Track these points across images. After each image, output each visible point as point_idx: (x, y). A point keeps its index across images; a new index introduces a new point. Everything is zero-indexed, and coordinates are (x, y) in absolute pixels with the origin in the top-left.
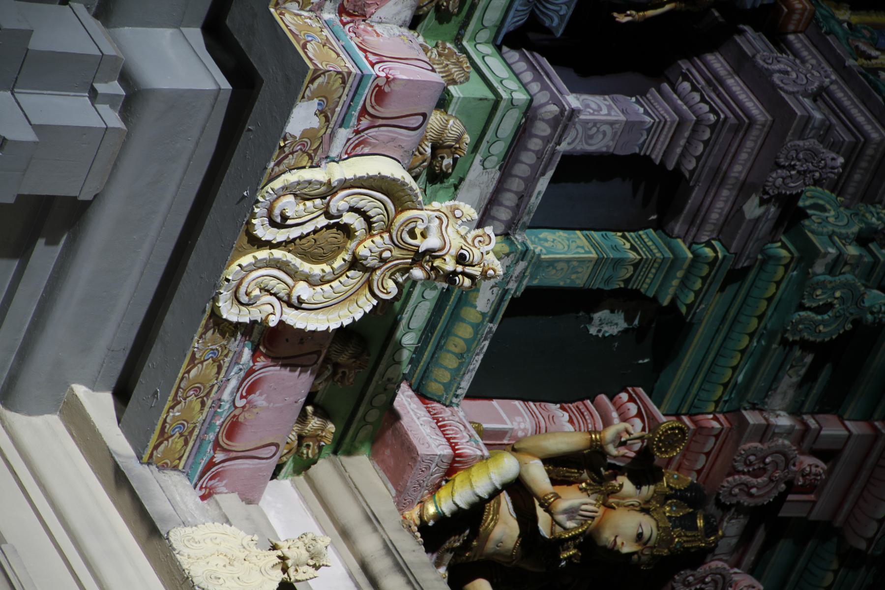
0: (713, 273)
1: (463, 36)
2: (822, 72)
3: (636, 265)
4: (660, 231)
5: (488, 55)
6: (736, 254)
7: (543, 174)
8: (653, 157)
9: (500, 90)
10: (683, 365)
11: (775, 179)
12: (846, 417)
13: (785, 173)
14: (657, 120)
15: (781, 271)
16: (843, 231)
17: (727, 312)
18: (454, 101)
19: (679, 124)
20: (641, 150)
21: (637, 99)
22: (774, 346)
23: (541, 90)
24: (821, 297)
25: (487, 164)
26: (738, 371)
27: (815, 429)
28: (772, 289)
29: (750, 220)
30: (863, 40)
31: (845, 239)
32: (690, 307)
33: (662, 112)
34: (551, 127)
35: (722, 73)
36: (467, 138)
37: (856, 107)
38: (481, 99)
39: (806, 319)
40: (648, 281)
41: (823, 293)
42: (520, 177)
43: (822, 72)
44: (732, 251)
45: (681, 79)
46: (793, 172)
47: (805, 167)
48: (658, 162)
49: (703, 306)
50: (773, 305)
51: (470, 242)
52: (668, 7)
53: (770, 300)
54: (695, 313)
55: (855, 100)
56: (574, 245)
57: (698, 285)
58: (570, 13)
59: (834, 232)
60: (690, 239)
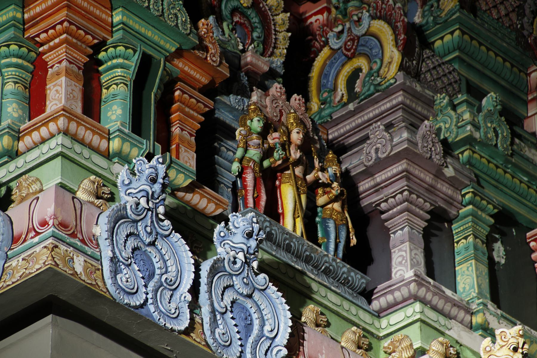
0: (480, 194)
1: (377, 336)
2: (377, 129)
3: (476, 237)
4: (453, 221)
5: (388, 322)
6: (471, 181)
7: (444, 292)
8: (424, 226)
9: (415, 318)
10: (518, 210)
11: (437, 159)
12: (526, 115)
13: (433, 154)
14: (407, 224)
15: (476, 155)
16: (455, 120)
17: (493, 185)
18: (423, 346)
19: (408, 211)
20: (420, 233)
21: (392, 233)
22: (513, 161)
23: (400, 291)
24: (491, 135)
25: (449, 328)
26: (522, 180)
27: (124, 33)
28: (484, 160)
29: (455, 173)
30: (333, 98)
31: (459, 119)
32: (495, 207)
33: (401, 220)
34: (421, 287)
35: (372, 183)
36: (441, 339)
37: (380, 107)
38: (421, 330)
39: (501, 143)
40: (482, 230)
41: (489, 133)
42: (444, 305)
43: (377, 129)
44: (469, 183)
45: (378, 208)
46: (433, 149)
47: (430, 142)
48: (426, 224)
49: (494, 200)
50: (492, 160)
51: (505, 343)
52: (347, 215)
53: (489, 162)
54: (498, 204)
55: (376, 107)
56: (466, 272)
57: (484, 202)
58: (360, 273)
59: (456, 125)
60: (459, 206)
